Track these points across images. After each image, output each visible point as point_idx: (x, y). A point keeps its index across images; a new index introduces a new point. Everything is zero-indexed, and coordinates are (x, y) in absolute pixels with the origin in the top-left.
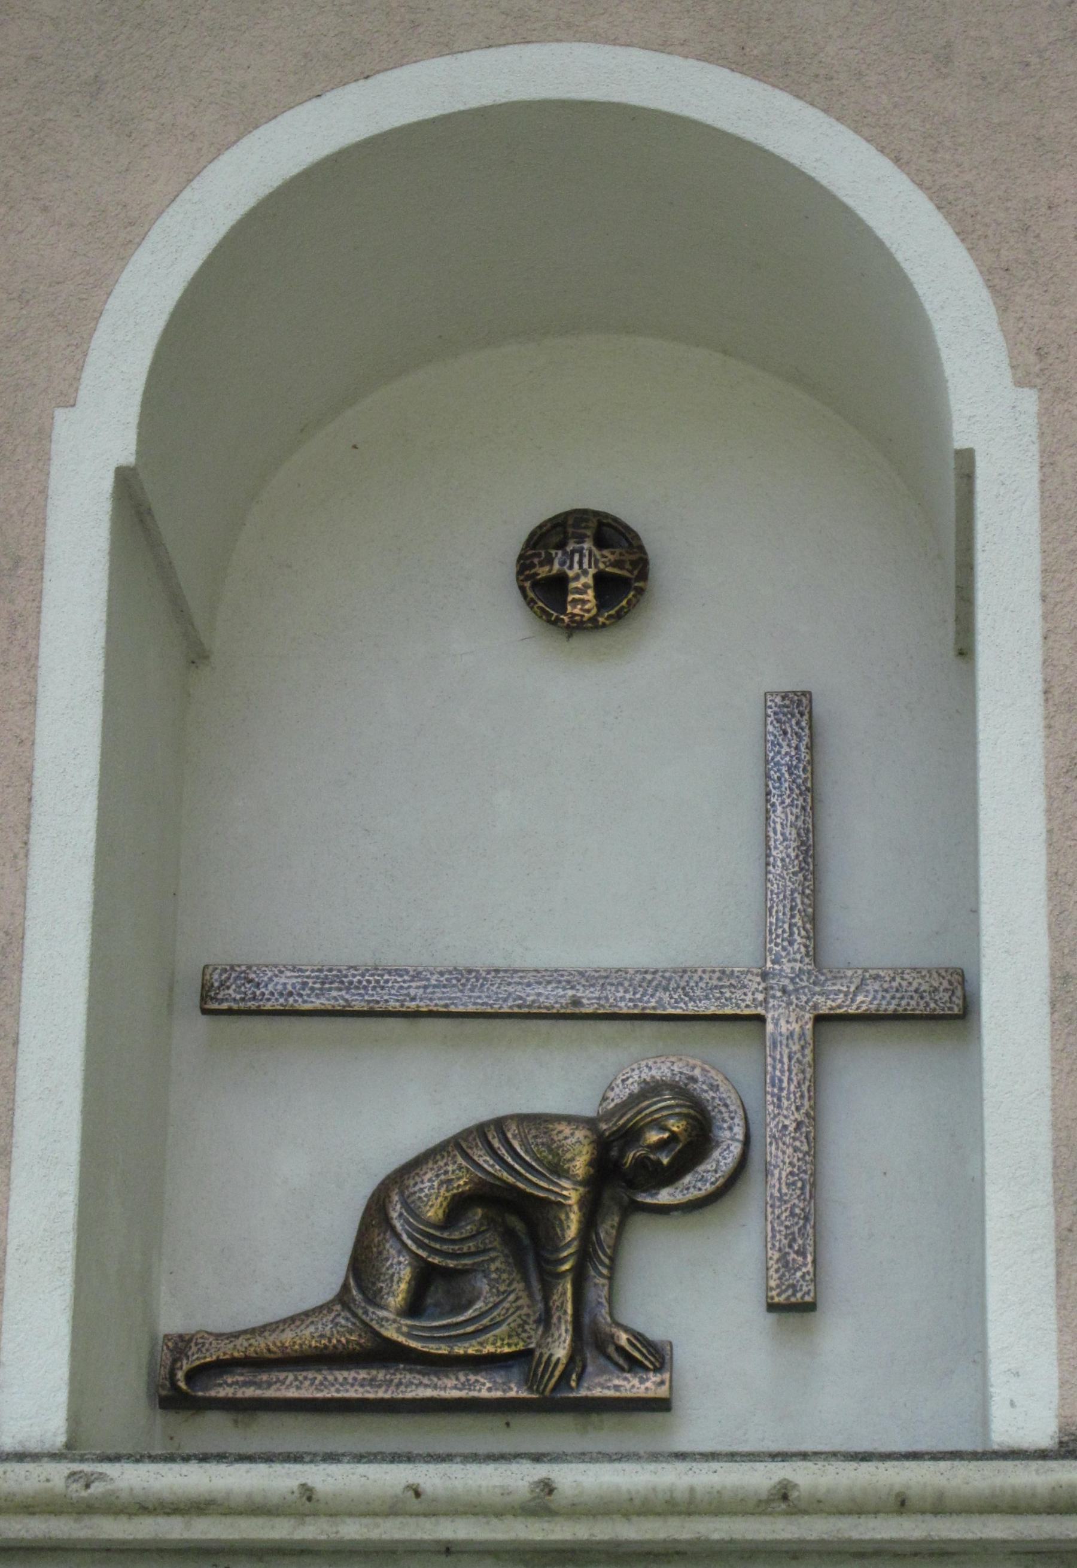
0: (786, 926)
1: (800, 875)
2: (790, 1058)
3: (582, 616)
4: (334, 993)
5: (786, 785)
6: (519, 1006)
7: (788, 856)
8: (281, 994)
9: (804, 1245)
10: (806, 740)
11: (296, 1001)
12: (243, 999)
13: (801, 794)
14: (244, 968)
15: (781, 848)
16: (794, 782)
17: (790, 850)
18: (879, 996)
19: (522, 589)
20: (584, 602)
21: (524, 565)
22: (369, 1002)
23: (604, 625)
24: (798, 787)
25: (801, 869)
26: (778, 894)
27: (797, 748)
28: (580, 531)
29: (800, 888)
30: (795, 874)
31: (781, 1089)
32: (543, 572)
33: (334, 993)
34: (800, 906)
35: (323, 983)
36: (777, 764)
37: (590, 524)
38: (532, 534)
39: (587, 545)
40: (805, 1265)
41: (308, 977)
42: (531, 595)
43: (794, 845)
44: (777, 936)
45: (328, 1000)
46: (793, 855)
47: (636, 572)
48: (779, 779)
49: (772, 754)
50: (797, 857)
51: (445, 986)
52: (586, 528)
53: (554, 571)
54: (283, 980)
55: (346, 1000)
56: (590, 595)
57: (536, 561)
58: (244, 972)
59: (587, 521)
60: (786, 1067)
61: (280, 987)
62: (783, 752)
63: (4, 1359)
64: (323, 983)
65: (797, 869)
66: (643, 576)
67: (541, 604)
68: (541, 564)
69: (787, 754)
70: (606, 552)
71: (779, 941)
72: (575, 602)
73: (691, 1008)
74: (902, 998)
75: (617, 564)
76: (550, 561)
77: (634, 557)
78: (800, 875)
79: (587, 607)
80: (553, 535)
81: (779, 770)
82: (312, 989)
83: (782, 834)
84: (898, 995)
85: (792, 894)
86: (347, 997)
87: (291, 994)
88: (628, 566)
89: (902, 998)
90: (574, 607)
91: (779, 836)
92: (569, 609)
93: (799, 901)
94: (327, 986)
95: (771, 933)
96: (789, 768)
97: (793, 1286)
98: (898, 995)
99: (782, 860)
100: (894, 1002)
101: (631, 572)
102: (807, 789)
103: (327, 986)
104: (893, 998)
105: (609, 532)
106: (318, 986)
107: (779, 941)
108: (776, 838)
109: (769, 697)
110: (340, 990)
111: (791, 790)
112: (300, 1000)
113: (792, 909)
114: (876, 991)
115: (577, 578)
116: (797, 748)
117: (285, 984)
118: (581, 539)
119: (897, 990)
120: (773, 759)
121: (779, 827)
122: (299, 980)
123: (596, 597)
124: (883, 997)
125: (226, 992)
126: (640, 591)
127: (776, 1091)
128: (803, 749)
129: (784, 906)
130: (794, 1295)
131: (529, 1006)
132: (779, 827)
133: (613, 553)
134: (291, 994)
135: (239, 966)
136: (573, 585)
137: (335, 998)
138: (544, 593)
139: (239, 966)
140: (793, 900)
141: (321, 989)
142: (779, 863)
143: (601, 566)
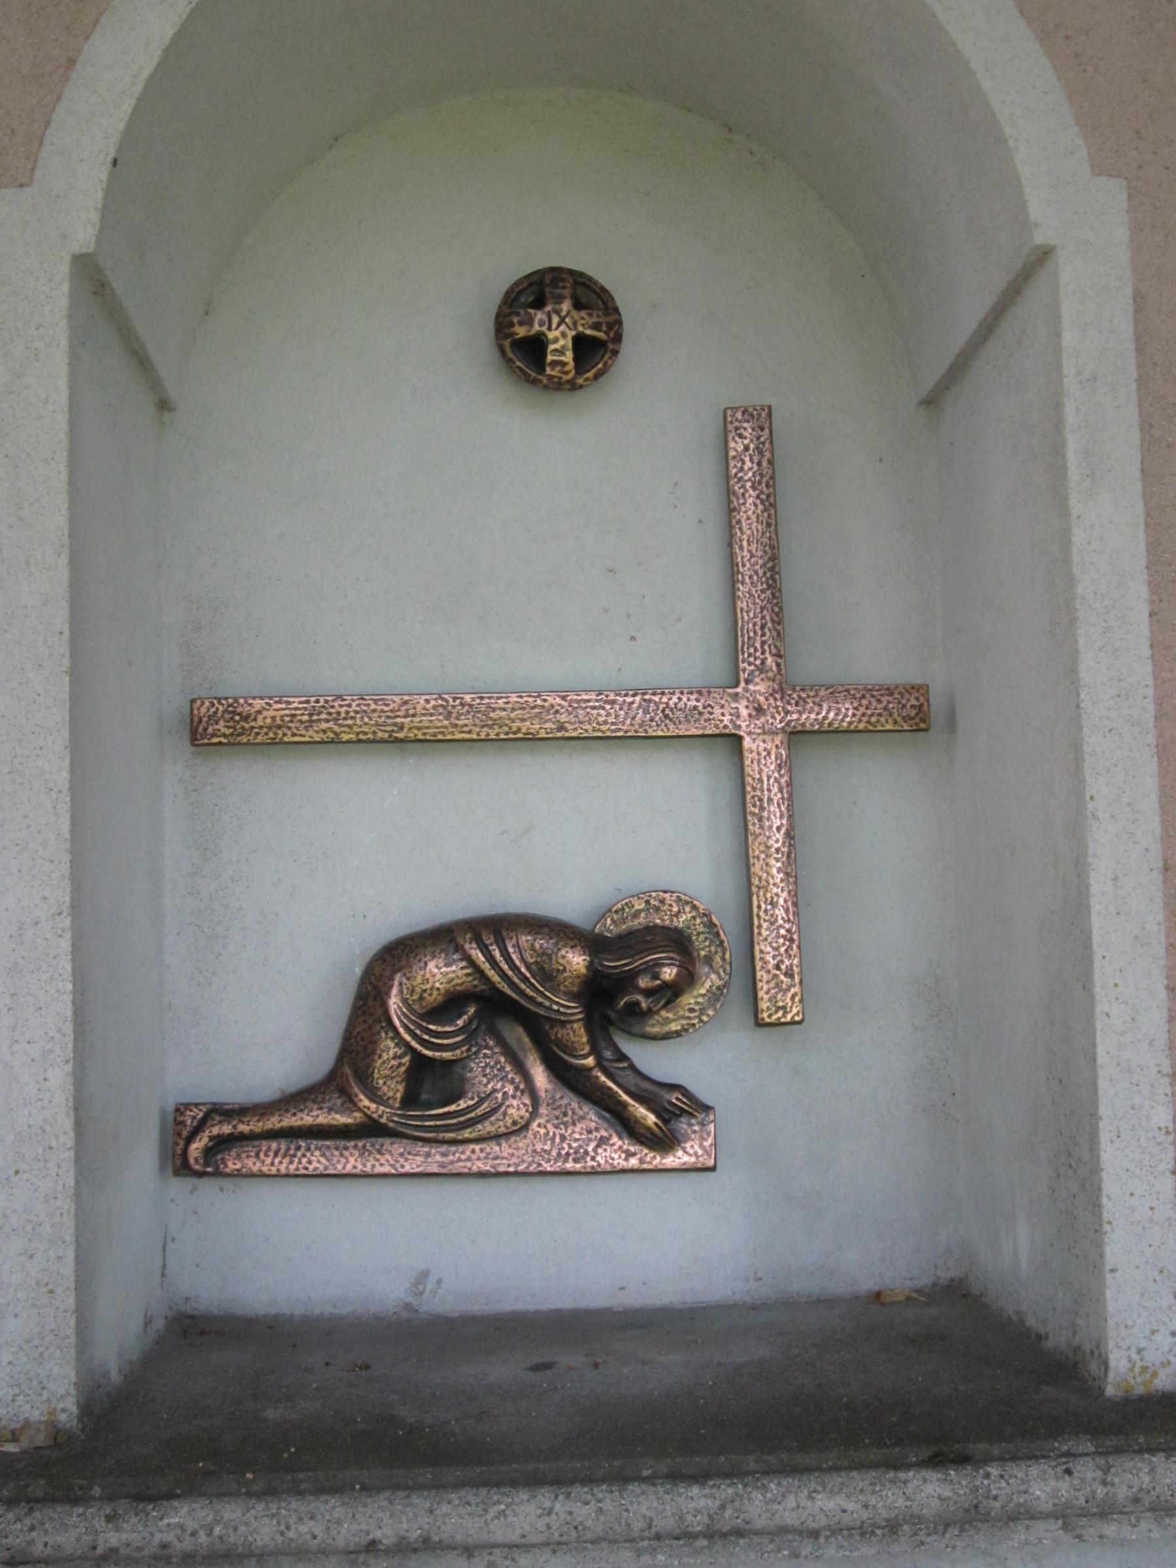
0: (758, 645)
1: (768, 592)
2: (769, 778)
3: (560, 378)
4: (324, 725)
5: (751, 500)
6: (507, 734)
7: (756, 573)
8: (270, 728)
9: (791, 965)
10: (768, 454)
11: (285, 735)
12: (232, 734)
13: (765, 510)
14: (231, 701)
15: (748, 565)
16: (758, 497)
17: (757, 567)
18: (850, 713)
19: (502, 351)
20: (564, 364)
21: (502, 325)
22: (358, 734)
23: (581, 386)
24: (762, 502)
25: (769, 586)
26: (748, 612)
27: (759, 464)
28: (559, 291)
29: (769, 606)
30: (763, 591)
31: (762, 808)
32: (521, 332)
33: (324, 725)
34: (770, 625)
35: (311, 715)
36: (740, 479)
37: (568, 285)
38: (508, 292)
39: (566, 306)
40: (794, 986)
41: (296, 709)
42: (510, 355)
43: (761, 562)
44: (750, 655)
45: (317, 732)
46: (761, 572)
47: (612, 334)
48: (743, 495)
49: (734, 471)
50: (765, 573)
51: (431, 715)
52: (564, 287)
53: (533, 332)
54: (272, 713)
55: (335, 733)
56: (569, 357)
57: (515, 320)
58: (231, 705)
59: (563, 280)
60: (765, 786)
61: (269, 721)
62: (746, 468)
63: (1169, 1181)
64: (311, 715)
65: (765, 586)
66: (618, 338)
67: (519, 364)
68: (521, 323)
69: (750, 469)
70: (583, 314)
71: (751, 659)
72: (554, 364)
73: (673, 731)
74: (872, 715)
75: (596, 326)
76: (530, 322)
77: (611, 319)
78: (768, 592)
79: (566, 369)
80: (538, 289)
81: (743, 487)
82: (301, 722)
83: (749, 551)
84: (869, 712)
85: (762, 612)
86: (336, 729)
87: (279, 727)
88: (604, 328)
89: (872, 715)
90: (553, 369)
91: (746, 553)
92: (548, 371)
93: (768, 618)
94: (315, 717)
95: (743, 653)
96: (753, 483)
97: (784, 1008)
98: (869, 712)
99: (751, 577)
100: (865, 719)
101: (606, 333)
102: (771, 505)
103: (315, 717)
104: (863, 715)
105: (588, 294)
106: (306, 718)
107: (751, 659)
108: (742, 555)
109: (729, 413)
110: (327, 721)
111: (756, 505)
112: (289, 733)
113: (762, 628)
114: (847, 709)
115: (556, 340)
116: (759, 464)
117: (273, 718)
118: (560, 299)
119: (867, 708)
120: (736, 474)
121: (745, 543)
122: (287, 712)
123: (576, 359)
124: (854, 715)
125: (216, 727)
126: (615, 353)
127: (757, 811)
128: (764, 464)
129: (755, 625)
130: (784, 1015)
131: (515, 733)
132: (745, 543)
133: (590, 315)
134: (279, 727)
135: (226, 699)
136: (551, 347)
137: (324, 731)
138: (525, 356)
139: (226, 699)
140: (763, 618)
141: (311, 721)
142: (747, 580)
143: (581, 329)
